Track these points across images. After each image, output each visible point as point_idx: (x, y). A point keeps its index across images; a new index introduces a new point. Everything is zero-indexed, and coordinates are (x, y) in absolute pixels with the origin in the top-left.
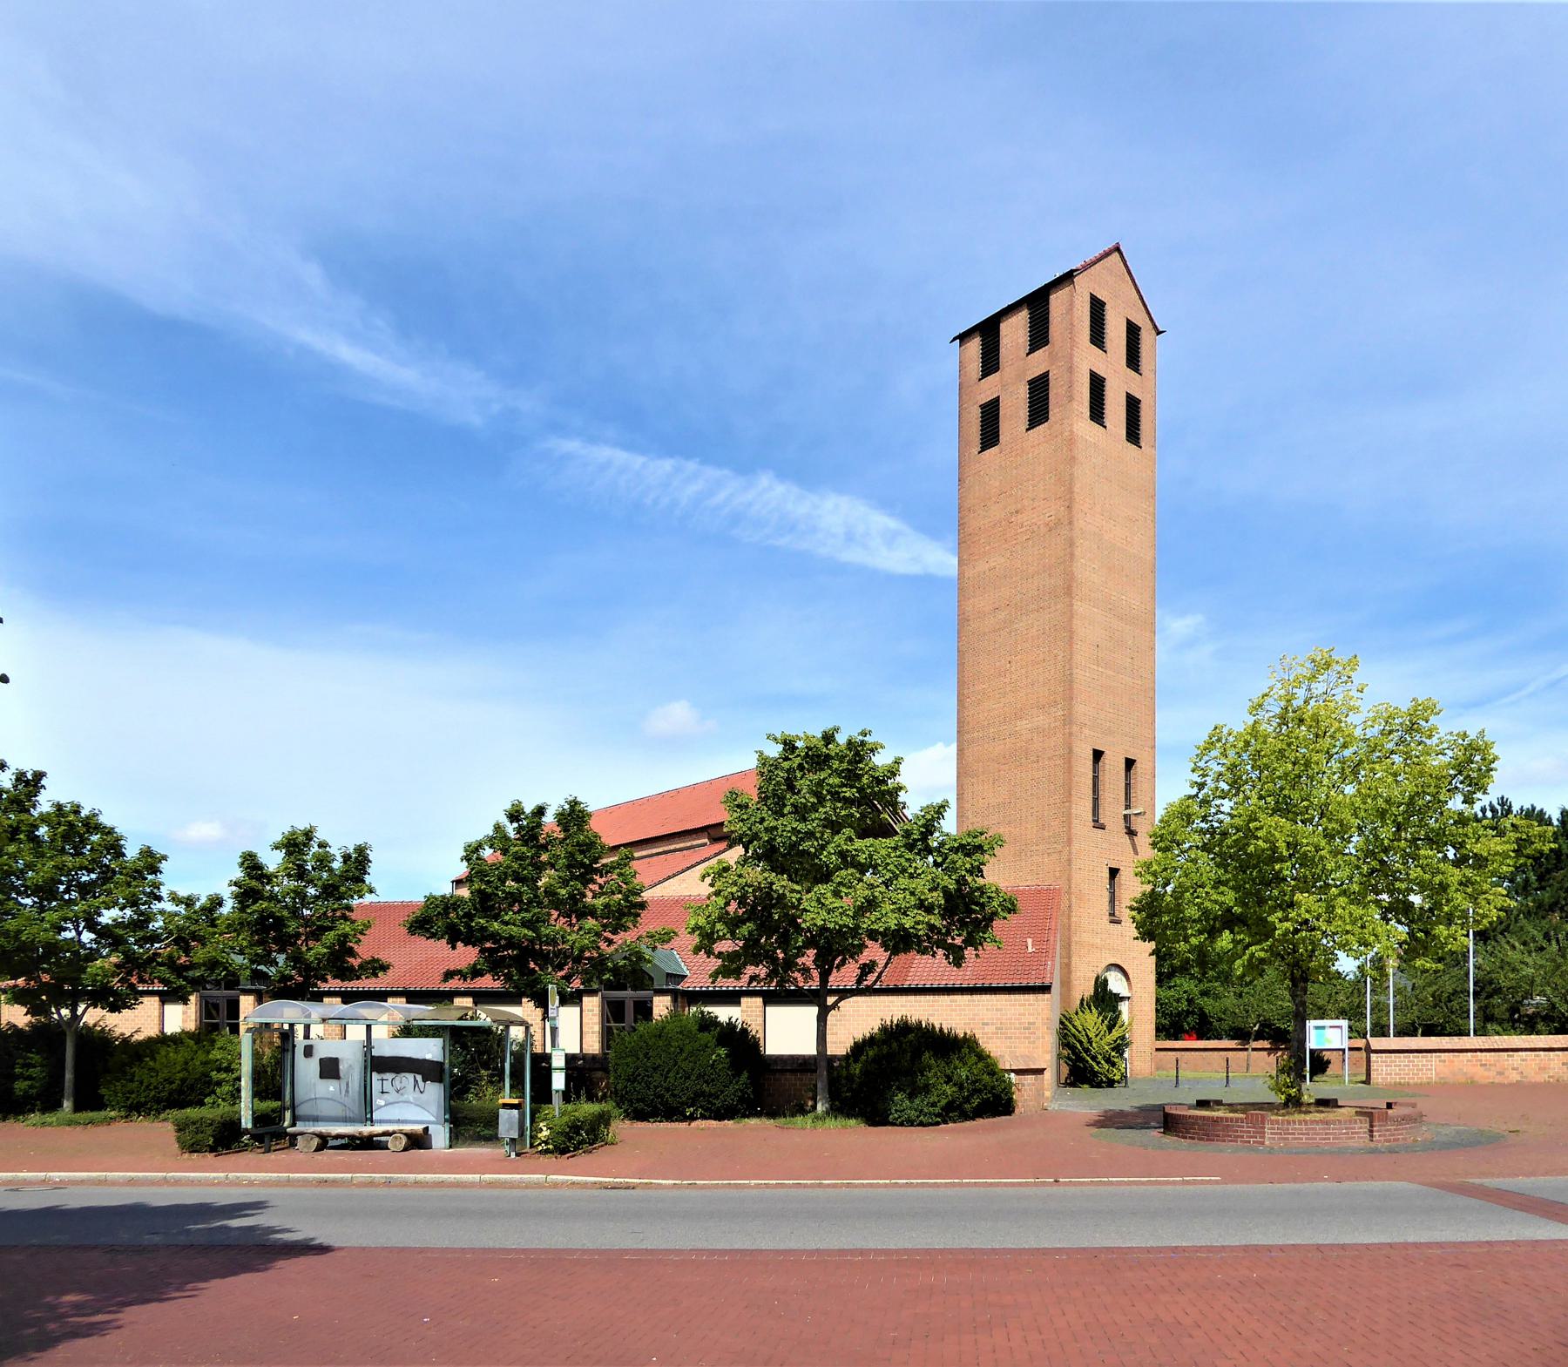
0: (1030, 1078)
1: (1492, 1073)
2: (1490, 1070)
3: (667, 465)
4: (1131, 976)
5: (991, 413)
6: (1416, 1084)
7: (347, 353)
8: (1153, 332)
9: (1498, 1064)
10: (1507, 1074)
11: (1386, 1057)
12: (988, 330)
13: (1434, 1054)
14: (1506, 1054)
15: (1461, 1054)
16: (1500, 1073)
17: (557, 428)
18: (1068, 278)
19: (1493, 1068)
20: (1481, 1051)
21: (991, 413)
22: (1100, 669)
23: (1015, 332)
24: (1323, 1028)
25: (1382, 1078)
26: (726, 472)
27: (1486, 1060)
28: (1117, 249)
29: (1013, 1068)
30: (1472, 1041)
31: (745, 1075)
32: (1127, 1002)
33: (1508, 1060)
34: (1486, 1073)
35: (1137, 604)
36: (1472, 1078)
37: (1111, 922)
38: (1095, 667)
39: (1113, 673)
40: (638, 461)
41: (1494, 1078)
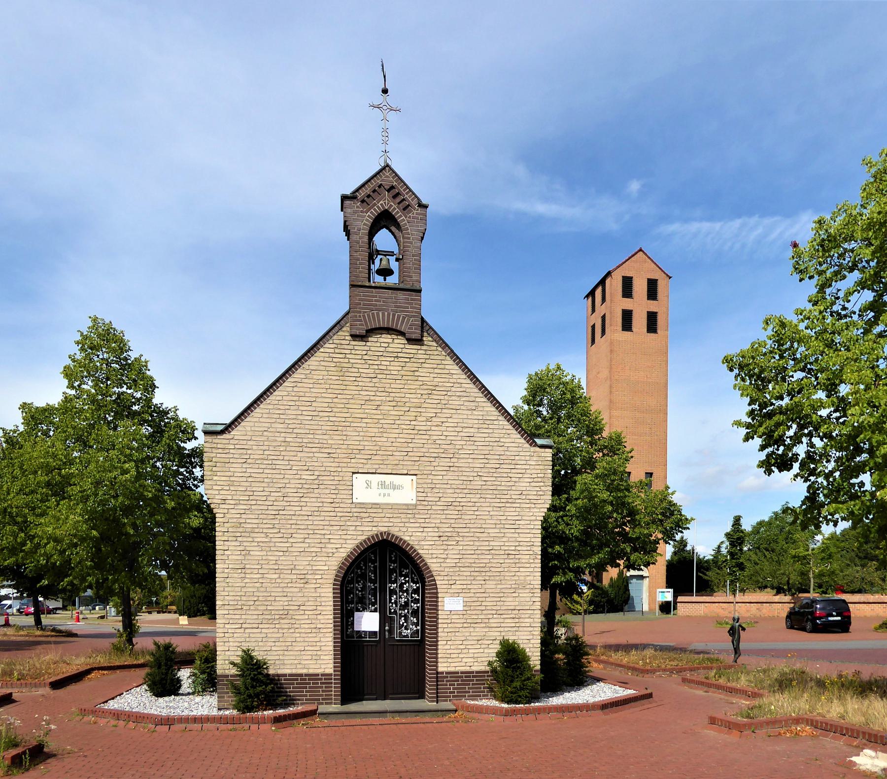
1: (727, 612)
3: (737, 223)
6: (695, 616)
7: (540, 208)
8: (668, 278)
12: (592, 294)
17: (666, 219)
18: (609, 274)
20: (722, 603)
24: (664, 592)
26: (776, 218)
28: (641, 250)
30: (695, 598)
32: (647, 579)
40: (717, 226)
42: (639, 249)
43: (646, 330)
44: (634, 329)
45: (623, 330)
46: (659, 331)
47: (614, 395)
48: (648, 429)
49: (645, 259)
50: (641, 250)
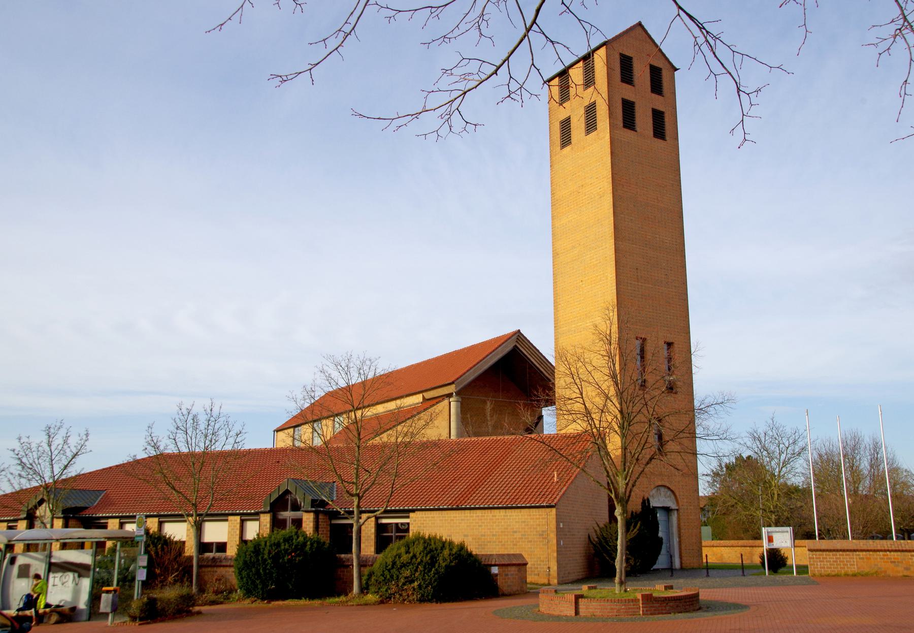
0: (513, 569)
5: (566, 125)
11: (819, 555)
12: (563, 74)
13: (855, 553)
14: (909, 554)
19: (900, 564)
21: (566, 125)
22: (640, 284)
23: (576, 75)
27: (894, 559)
29: (497, 563)
35: (669, 239)
38: (636, 283)
39: (650, 286)
43: (652, 133)
45: (624, 126)
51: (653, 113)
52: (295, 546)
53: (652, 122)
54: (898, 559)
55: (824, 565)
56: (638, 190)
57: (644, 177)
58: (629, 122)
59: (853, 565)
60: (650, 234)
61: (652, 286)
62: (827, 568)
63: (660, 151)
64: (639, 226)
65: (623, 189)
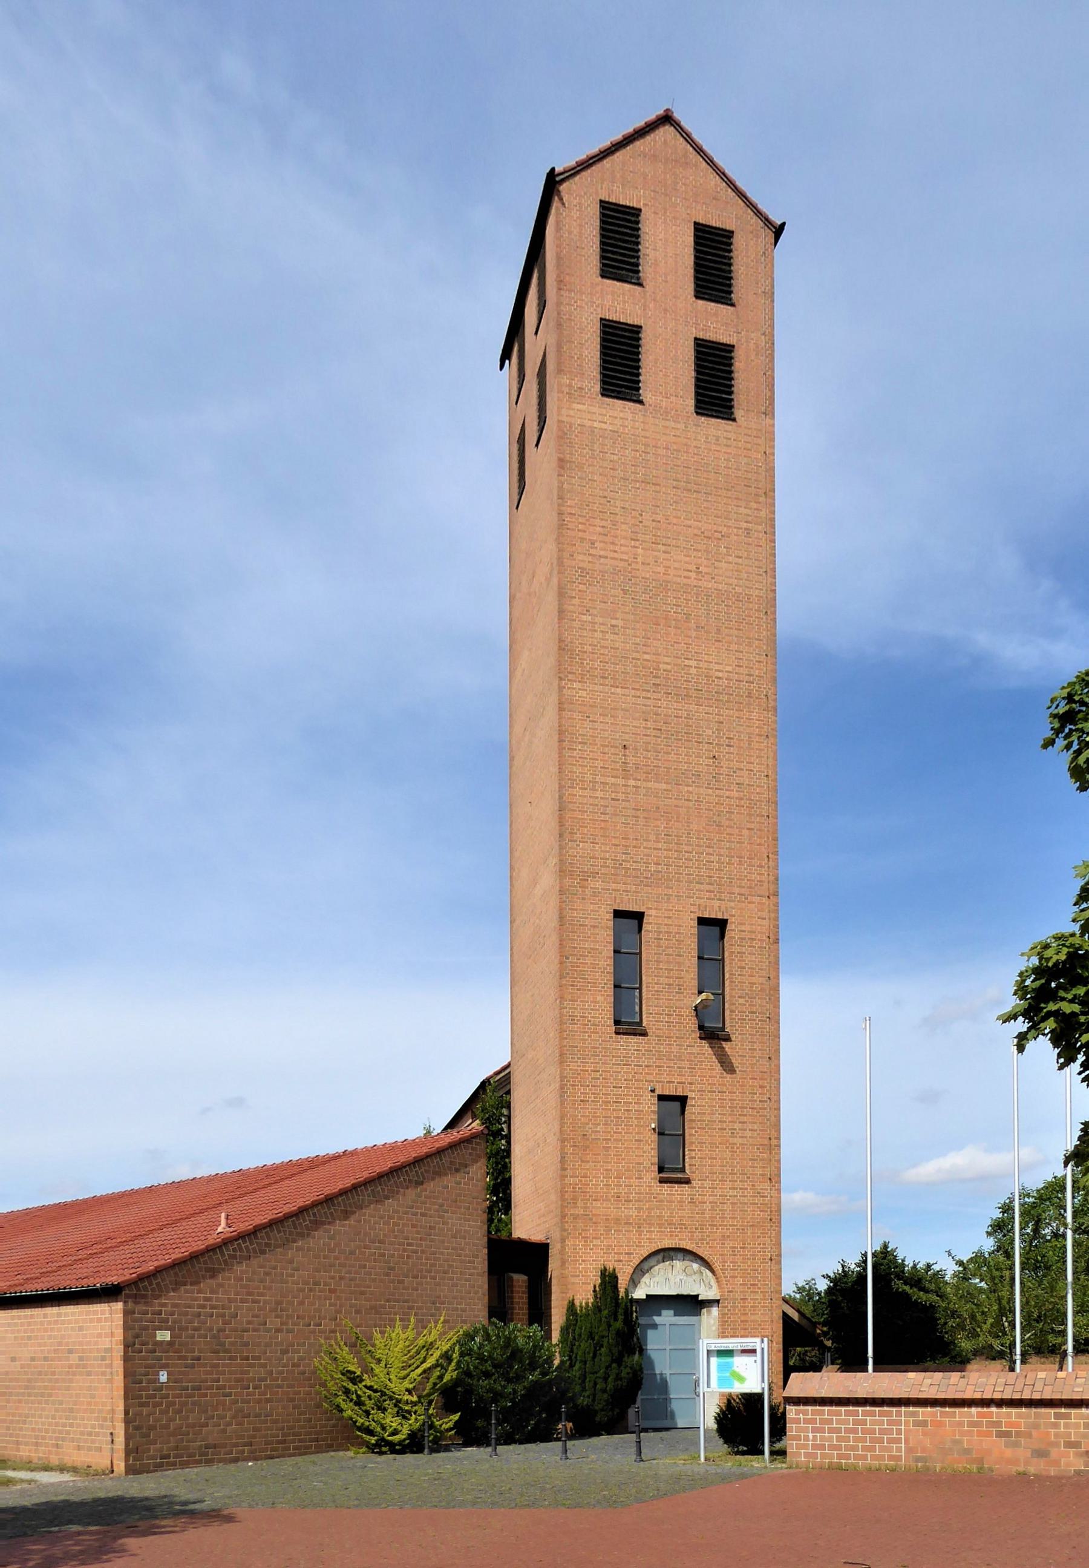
1: (1023, 1453)
2: (1016, 1445)
4: (717, 1266)
9: (1034, 1433)
10: (1054, 1453)
14: (1052, 1411)
15: (1073, 1411)
16: (1040, 1454)
20: (1000, 1403)
22: (631, 782)
24: (728, 1353)
25: (807, 1455)
28: (667, 119)
31: (456, 1417)
32: (715, 1311)
33: (1056, 1426)
34: (1009, 1453)
35: (729, 668)
36: (980, 1461)
37: (660, 1182)
38: (620, 781)
39: (664, 786)
41: (1027, 1463)
42: (660, 112)
43: (691, 402)
44: (646, 393)
45: (606, 392)
46: (738, 413)
47: (577, 624)
48: (704, 761)
49: (685, 155)
50: (667, 119)
51: (697, 352)
52: (560, 1413)
53: (693, 374)
54: (1018, 1425)
55: (822, 1439)
56: (640, 551)
57: (659, 517)
58: (713, 369)
59: (899, 1441)
60: (667, 660)
61: (669, 787)
62: (832, 1447)
63: (714, 447)
64: (638, 640)
65: (592, 551)
